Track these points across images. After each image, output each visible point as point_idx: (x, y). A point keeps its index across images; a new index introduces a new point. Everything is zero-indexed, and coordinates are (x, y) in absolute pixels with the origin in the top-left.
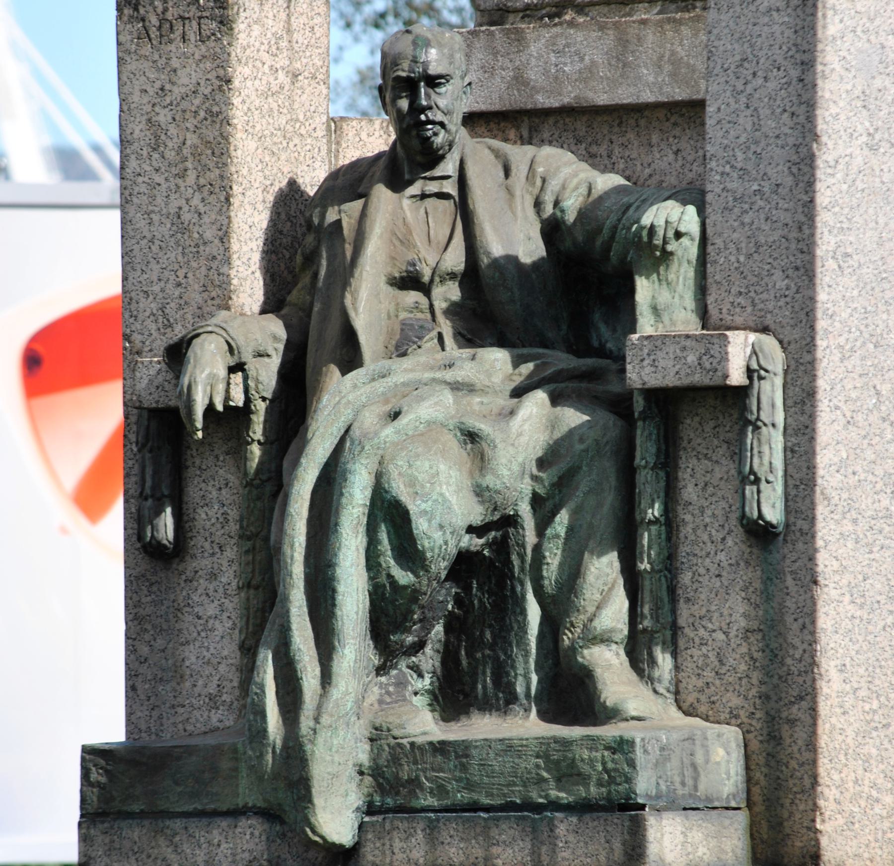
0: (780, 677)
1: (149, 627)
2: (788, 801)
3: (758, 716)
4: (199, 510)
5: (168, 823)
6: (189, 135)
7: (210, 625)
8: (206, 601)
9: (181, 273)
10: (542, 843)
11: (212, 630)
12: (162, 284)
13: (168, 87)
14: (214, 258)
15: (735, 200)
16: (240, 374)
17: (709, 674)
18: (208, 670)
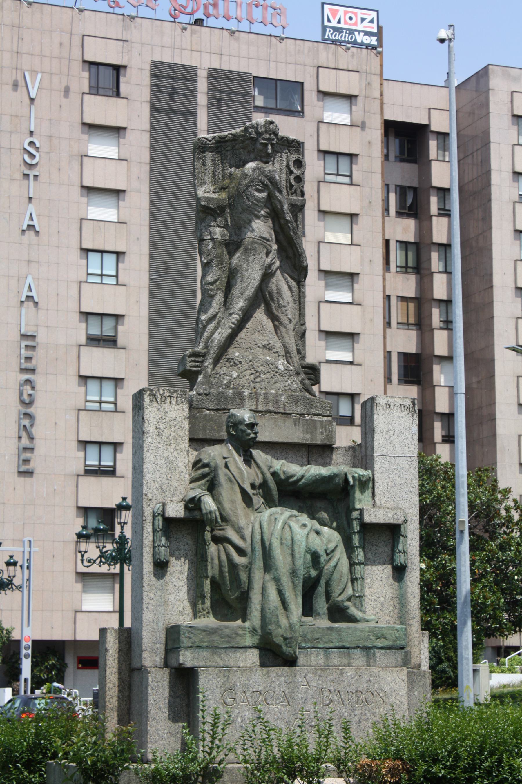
3: (397, 622)
7: (180, 588)
9: (169, 476)
16: (167, 515)
18: (178, 603)
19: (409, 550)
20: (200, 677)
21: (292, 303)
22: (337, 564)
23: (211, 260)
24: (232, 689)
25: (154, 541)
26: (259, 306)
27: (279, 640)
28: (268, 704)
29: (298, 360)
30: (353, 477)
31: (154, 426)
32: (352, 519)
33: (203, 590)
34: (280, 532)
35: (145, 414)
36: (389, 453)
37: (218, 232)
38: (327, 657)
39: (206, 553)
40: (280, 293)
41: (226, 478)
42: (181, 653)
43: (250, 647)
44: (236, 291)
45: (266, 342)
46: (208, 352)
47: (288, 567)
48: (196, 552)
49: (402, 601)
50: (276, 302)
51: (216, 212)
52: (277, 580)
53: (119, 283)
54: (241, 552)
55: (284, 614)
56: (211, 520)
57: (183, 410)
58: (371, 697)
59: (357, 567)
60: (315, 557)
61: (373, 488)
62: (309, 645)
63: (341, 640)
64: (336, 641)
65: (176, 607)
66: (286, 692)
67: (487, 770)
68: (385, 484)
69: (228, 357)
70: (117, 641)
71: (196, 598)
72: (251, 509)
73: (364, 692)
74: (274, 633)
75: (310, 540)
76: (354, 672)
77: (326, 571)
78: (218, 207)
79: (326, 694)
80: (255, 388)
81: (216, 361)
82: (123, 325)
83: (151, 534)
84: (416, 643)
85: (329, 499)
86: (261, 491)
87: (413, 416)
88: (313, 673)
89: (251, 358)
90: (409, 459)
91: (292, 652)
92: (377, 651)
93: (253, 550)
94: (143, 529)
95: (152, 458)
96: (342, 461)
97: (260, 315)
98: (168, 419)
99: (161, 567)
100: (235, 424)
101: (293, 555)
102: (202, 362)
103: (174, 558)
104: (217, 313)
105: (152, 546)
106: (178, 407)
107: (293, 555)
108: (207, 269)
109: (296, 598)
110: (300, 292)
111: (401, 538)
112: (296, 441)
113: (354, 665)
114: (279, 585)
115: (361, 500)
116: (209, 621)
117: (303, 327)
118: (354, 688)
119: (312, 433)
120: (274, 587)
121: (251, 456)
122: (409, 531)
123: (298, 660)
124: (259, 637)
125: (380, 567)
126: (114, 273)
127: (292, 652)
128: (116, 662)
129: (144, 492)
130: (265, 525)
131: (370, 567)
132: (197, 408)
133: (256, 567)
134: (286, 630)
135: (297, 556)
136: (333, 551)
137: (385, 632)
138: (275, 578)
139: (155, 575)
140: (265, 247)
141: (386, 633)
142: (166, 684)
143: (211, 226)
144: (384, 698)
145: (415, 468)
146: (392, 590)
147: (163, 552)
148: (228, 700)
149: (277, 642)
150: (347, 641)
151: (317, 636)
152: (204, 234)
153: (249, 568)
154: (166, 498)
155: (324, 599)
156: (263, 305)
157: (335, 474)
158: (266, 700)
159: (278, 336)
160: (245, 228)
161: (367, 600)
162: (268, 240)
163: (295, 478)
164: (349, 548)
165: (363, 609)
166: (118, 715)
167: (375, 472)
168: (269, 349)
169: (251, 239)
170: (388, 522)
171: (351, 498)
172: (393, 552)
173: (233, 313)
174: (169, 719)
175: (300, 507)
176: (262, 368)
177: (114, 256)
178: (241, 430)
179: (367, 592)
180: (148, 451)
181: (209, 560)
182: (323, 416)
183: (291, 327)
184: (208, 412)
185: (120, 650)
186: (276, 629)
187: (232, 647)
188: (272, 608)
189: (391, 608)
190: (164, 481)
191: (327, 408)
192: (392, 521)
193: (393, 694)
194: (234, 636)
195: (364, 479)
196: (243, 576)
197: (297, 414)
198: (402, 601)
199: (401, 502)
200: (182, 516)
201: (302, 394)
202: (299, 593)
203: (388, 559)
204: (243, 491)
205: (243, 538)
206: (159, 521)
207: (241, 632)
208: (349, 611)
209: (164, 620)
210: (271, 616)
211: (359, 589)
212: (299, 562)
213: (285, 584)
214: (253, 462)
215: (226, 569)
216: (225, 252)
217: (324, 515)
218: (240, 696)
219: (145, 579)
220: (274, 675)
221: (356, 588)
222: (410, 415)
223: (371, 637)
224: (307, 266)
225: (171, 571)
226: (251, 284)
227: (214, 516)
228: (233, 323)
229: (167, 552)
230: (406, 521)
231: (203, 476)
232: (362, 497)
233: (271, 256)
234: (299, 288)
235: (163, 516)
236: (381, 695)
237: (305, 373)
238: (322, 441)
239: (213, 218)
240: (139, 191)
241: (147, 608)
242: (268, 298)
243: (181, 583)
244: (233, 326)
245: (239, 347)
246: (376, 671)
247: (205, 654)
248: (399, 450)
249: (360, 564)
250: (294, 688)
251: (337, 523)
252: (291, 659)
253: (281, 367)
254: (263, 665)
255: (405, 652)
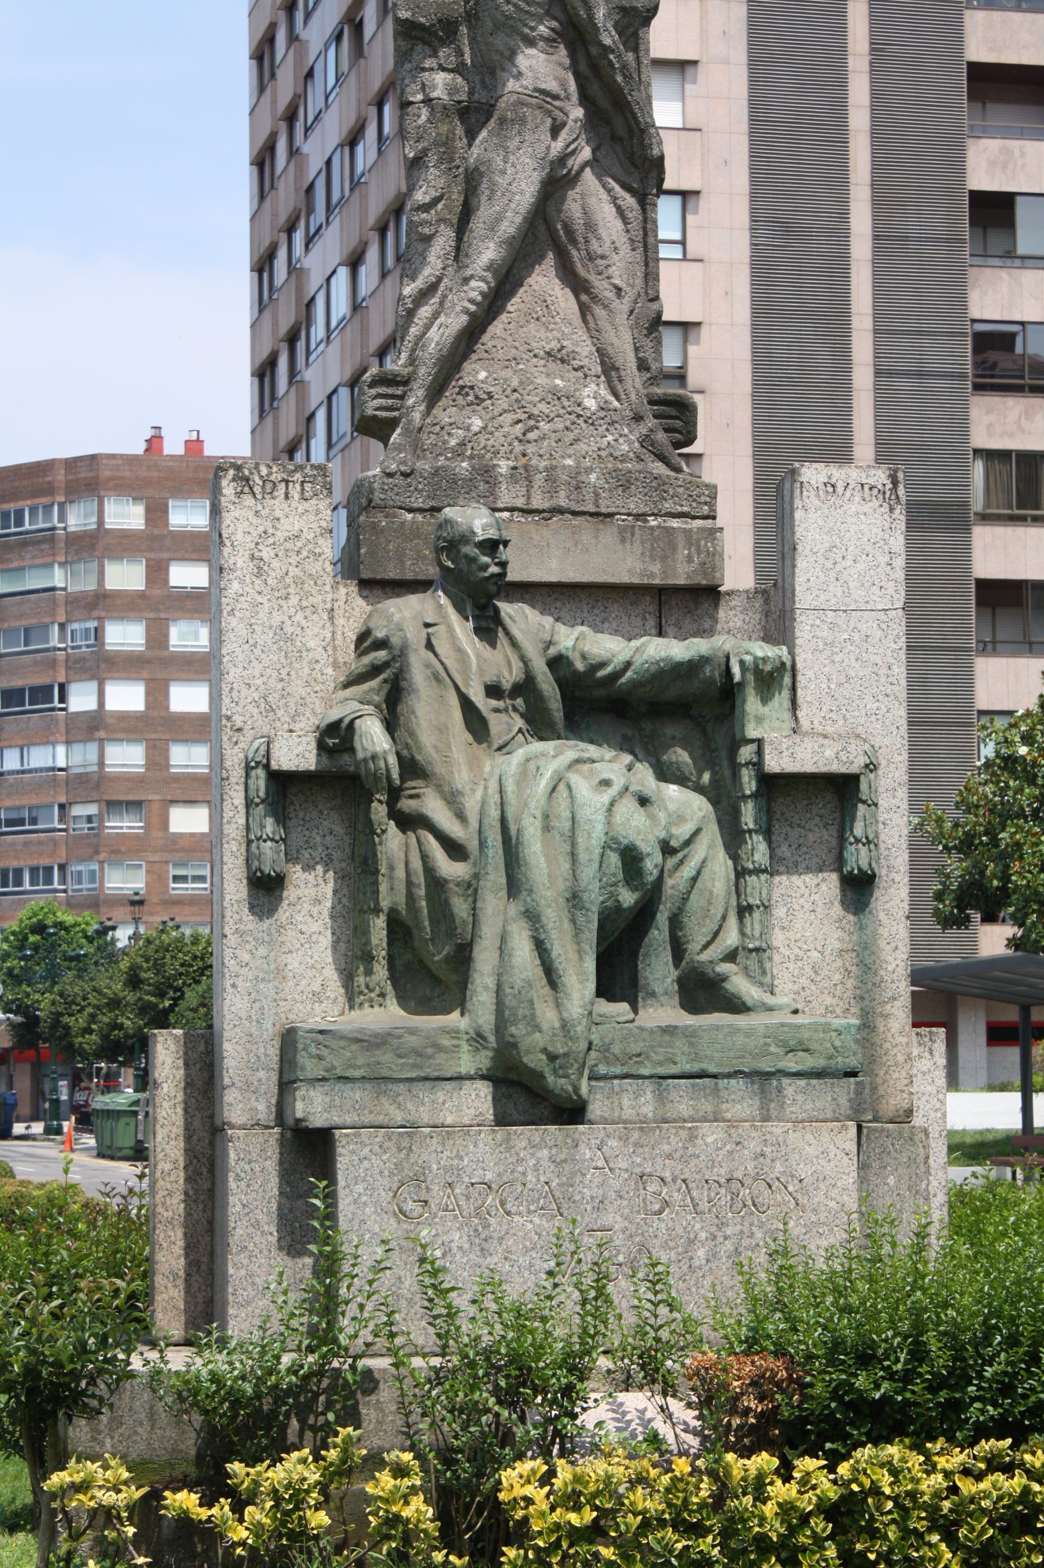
0: (874, 984)
1: (251, 939)
2: (882, 1073)
3: (853, 1010)
4: (303, 851)
5: (390, 1086)
6: (291, 569)
7: (314, 938)
8: (310, 919)
9: (284, 672)
10: (771, 1101)
11: (316, 942)
12: (265, 679)
13: (270, 531)
14: (317, 661)
15: (826, 644)
16: (274, 766)
17: (804, 981)
18: (310, 973)
19: (882, 837)
20: (339, 1150)
21: (625, 249)
22: (699, 873)
23: (425, 152)
24: (419, 1179)
25: (248, 828)
26: (540, 258)
27: (535, 1060)
28: (508, 1213)
29: (639, 385)
30: (742, 663)
31: (247, 554)
32: (741, 765)
33: (368, 942)
34: (543, 801)
35: (223, 526)
36: (833, 602)
37: (441, 83)
38: (661, 1099)
39: (375, 854)
40: (590, 226)
41: (429, 672)
42: (298, 1094)
43: (470, 1078)
44: (478, 224)
45: (554, 345)
46: (414, 372)
47: (562, 885)
48: (353, 853)
49: (864, 961)
50: (582, 246)
51: (436, 35)
52: (532, 917)
53: (689, 257)
54: (455, 849)
55: (550, 999)
56: (375, 774)
57: (318, 512)
58: (767, 1192)
59: (751, 880)
60: (631, 858)
61: (794, 689)
62: (618, 1070)
63: (697, 1058)
64: (684, 1059)
65: (304, 982)
66: (554, 1184)
67: (998, 1382)
68: (824, 678)
69: (461, 382)
70: (181, 1063)
71: (353, 959)
72: (485, 745)
73: (748, 1181)
74: (525, 1044)
75: (618, 818)
76: (722, 1135)
77: (670, 892)
78: (440, 21)
79: (652, 1188)
80: (524, 455)
81: (435, 394)
82: (697, 342)
83: (243, 811)
84: (901, 1058)
85: (682, 717)
86: (519, 701)
87: (892, 510)
88: (620, 1139)
89: (515, 383)
90: (882, 616)
91: (570, 1089)
92: (785, 1081)
93: (482, 844)
94: (222, 800)
95: (243, 631)
96: (739, 624)
97: (544, 280)
98: (280, 535)
99: (266, 888)
100: (452, 543)
101: (573, 855)
102: (402, 397)
103: (298, 867)
104: (439, 279)
105: (243, 840)
106: (306, 505)
107: (573, 855)
108: (415, 173)
109: (581, 958)
110: (645, 220)
111: (861, 807)
112: (626, 579)
113: (728, 1115)
114: (536, 929)
115: (763, 720)
116: (387, 1015)
117: (654, 306)
118: (723, 1171)
119: (663, 559)
120: (526, 934)
121: (497, 619)
122: (881, 789)
123: (590, 1107)
124: (490, 1054)
125: (809, 879)
126: (678, 236)
127: (570, 1089)
128: (180, 1111)
129: (224, 711)
130: (510, 787)
131: (784, 878)
132: (382, 508)
133: (489, 885)
134: (554, 1035)
135: (583, 857)
136: (688, 843)
137: (806, 1035)
138: (527, 911)
139: (252, 908)
140: (549, 113)
141: (810, 1040)
142: (271, 1165)
143: (424, 70)
144: (799, 1196)
145: (898, 636)
146: (840, 933)
147: (268, 852)
148: (409, 1206)
149: (532, 1065)
150: (711, 1059)
151: (636, 1048)
152: (408, 89)
153: (471, 888)
154: (278, 724)
155: (667, 956)
156: (551, 255)
157: (702, 657)
158: (503, 1203)
159: (588, 329)
160: (503, 70)
161: (777, 958)
162: (556, 97)
163: (609, 669)
164: (733, 838)
165: (768, 979)
166: (185, 1234)
167: (798, 650)
168: (563, 361)
169: (515, 96)
170: (824, 769)
171: (737, 712)
172: (842, 840)
173: (472, 277)
174: (280, 1248)
175: (625, 737)
176: (542, 406)
177: (677, 200)
178: (466, 556)
179: (778, 938)
180: (232, 613)
181: (383, 871)
182: (694, 518)
183: (622, 307)
184: (409, 516)
185: (189, 1085)
186: (528, 1034)
187: (426, 1079)
188: (519, 984)
189: (837, 977)
190: (272, 683)
191: (703, 499)
192: (835, 768)
193: (822, 1186)
194: (430, 1051)
195: (768, 668)
196: (460, 907)
197: (629, 515)
198: (864, 961)
199: (862, 722)
200: (313, 768)
201: (639, 466)
202: (587, 948)
203: (830, 859)
204: (467, 705)
205: (461, 817)
206: (260, 781)
207: (446, 1042)
208: (727, 985)
209: (276, 1014)
210: (514, 1003)
211: (757, 933)
212: (588, 872)
213: (551, 925)
214: (501, 633)
215: (422, 892)
216: (460, 130)
217: (681, 756)
218: (437, 1194)
219: (227, 919)
220: (524, 1144)
221: (748, 931)
222: (886, 507)
223: (773, 1049)
224: (661, 158)
225: (292, 899)
226: (513, 205)
227: (382, 765)
228: (472, 301)
229: (278, 852)
230: (871, 767)
231: (375, 670)
232: (766, 710)
233: (564, 136)
234: (644, 210)
235: (267, 766)
236: (791, 1188)
237: (655, 417)
238: (689, 577)
239: (428, 50)
240: (726, 62)
241: (234, 986)
242: (564, 238)
243: (315, 927)
244: (473, 308)
245: (489, 359)
246: (778, 1131)
247: (357, 1096)
248: (859, 594)
249: (758, 871)
250: (573, 1174)
251: (714, 774)
252: (568, 1106)
253: (591, 404)
254: (502, 1120)
255: (857, 1083)
